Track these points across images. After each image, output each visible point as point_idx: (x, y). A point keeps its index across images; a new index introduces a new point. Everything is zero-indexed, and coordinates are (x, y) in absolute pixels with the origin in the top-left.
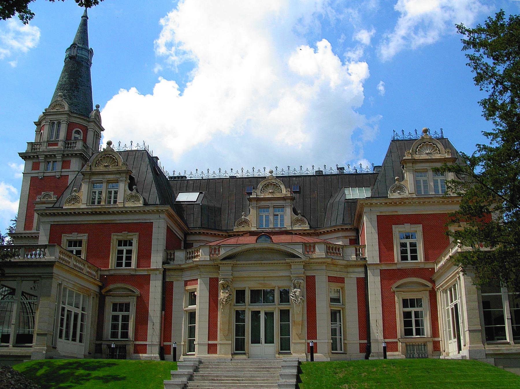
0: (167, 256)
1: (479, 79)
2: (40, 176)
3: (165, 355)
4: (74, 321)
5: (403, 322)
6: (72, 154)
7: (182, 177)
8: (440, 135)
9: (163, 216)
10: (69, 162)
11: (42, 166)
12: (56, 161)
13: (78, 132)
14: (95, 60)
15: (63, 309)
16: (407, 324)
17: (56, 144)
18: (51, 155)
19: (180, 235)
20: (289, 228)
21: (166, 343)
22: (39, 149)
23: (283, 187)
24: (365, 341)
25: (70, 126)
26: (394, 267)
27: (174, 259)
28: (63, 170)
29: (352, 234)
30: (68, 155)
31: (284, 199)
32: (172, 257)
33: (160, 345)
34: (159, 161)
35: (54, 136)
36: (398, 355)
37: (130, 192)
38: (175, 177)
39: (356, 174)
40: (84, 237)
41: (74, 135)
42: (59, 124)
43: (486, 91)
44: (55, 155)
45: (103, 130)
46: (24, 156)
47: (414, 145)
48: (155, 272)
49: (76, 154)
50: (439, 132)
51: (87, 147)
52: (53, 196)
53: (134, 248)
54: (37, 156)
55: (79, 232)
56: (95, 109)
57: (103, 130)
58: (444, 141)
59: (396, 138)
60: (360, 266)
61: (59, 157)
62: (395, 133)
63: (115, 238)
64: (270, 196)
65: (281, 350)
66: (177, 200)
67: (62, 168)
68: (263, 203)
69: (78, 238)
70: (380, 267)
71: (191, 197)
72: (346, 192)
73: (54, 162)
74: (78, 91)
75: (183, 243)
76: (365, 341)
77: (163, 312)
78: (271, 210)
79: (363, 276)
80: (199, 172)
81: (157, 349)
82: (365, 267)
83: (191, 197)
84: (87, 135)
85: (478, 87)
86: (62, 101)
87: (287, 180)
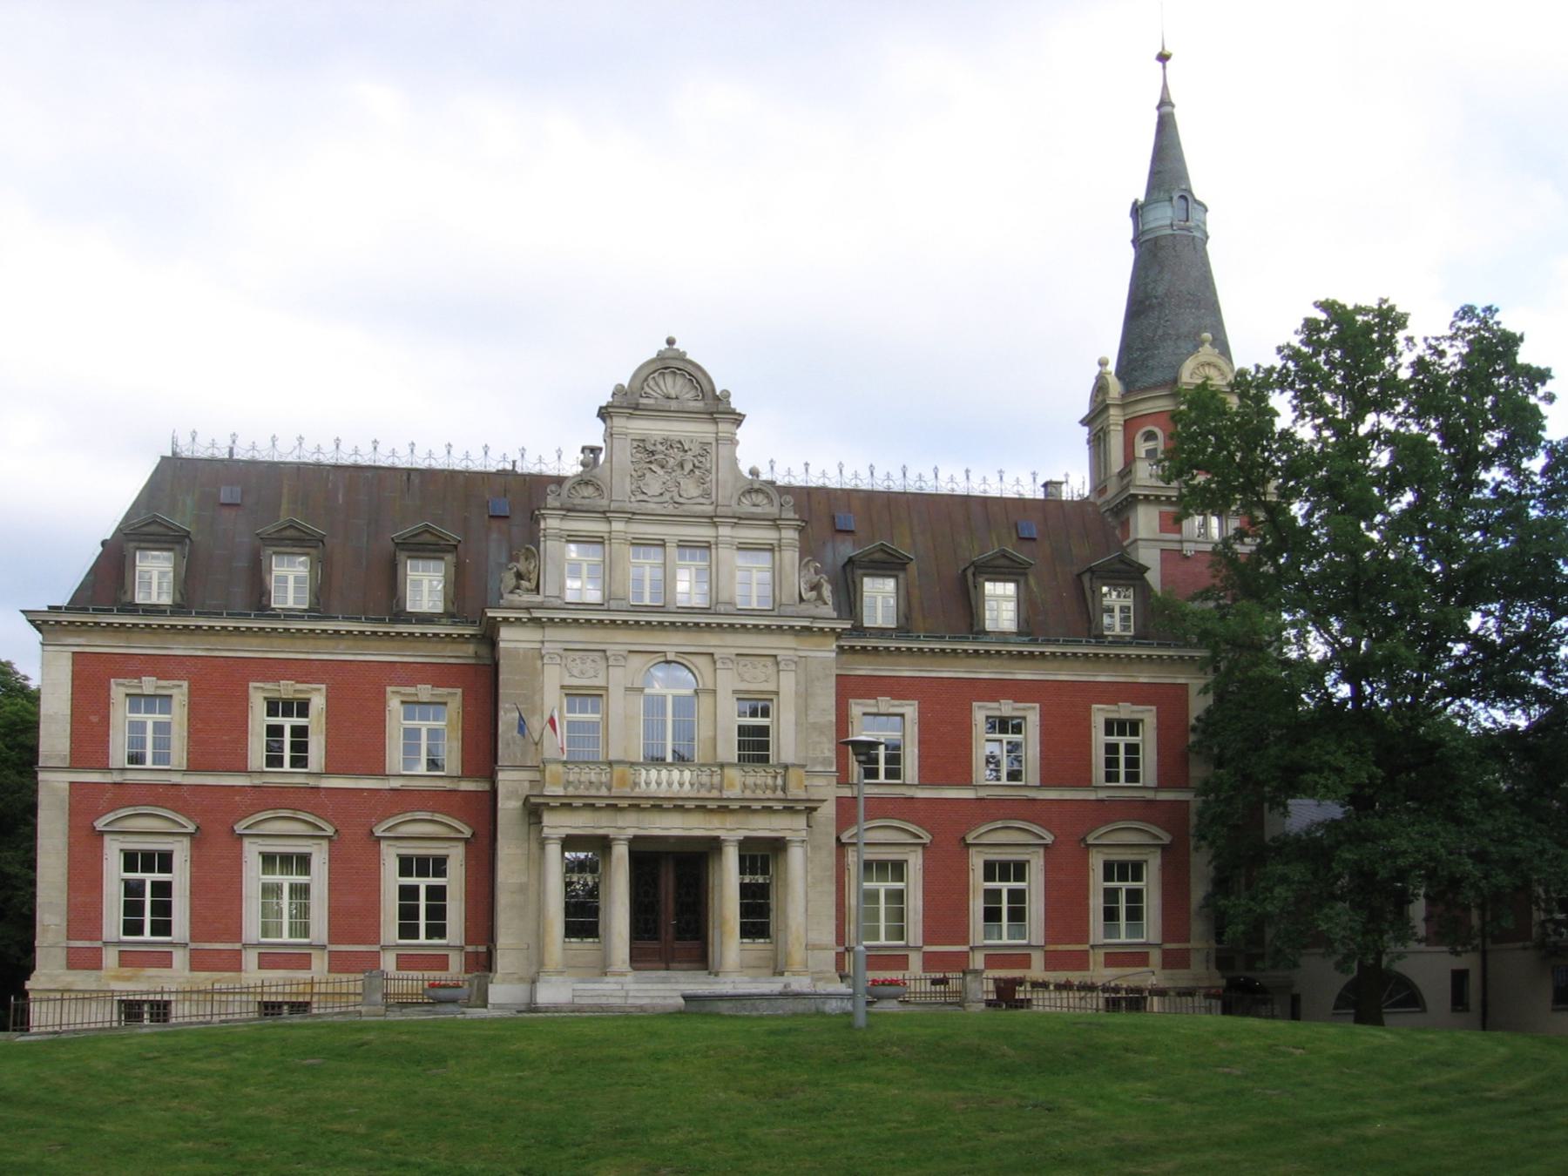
26: (1092, 796)
63: (980, 714)
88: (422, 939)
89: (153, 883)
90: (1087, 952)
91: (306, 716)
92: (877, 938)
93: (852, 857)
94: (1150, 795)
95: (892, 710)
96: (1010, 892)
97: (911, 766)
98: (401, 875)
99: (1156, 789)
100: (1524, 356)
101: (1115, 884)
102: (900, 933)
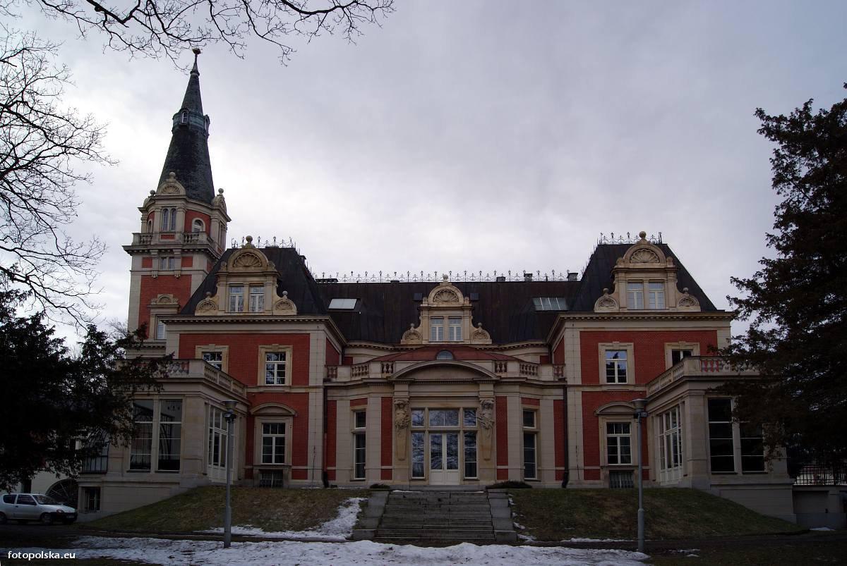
0: (383, 368)
1: (778, 181)
2: (155, 274)
3: (329, 481)
4: (215, 444)
5: (708, 426)
6: (194, 250)
7: (333, 280)
8: (658, 240)
9: (322, 327)
10: (192, 258)
11: (156, 264)
12: (173, 258)
13: (199, 222)
14: (212, 130)
15: (211, 431)
16: (612, 450)
17: (173, 237)
18: (166, 250)
19: (338, 348)
20: (467, 342)
21: (329, 468)
22: (150, 241)
23: (460, 295)
24: (563, 468)
25: (189, 215)
26: (598, 389)
27: (336, 376)
28: (183, 269)
29: (544, 351)
30: (189, 250)
31: (462, 308)
32: (334, 373)
33: (323, 470)
34: (306, 261)
35: (168, 226)
36: (600, 484)
37: (279, 298)
38: (324, 280)
39: (547, 283)
40: (224, 350)
41: (195, 226)
42: (174, 210)
43: (788, 193)
44: (171, 250)
45: (229, 220)
46: (129, 250)
47: (630, 251)
48: (314, 390)
49: (200, 250)
50: (657, 236)
51: (210, 240)
52: (172, 300)
53: (288, 362)
54: (149, 250)
55: (217, 344)
56: (218, 193)
57: (229, 220)
58: (665, 249)
59: (603, 242)
60: (558, 387)
61: (177, 253)
62: (603, 236)
63: (262, 350)
64: (445, 305)
65: (466, 476)
66: (330, 307)
67: (182, 266)
68: (436, 313)
69: (216, 351)
70: (582, 389)
71: (350, 304)
72: (536, 302)
73: (170, 258)
74: (195, 171)
75: (340, 356)
76: (563, 468)
77: (326, 434)
78: (446, 321)
79: (562, 398)
80: (355, 275)
81: (319, 474)
82: (565, 388)
83: (350, 304)
84: (210, 226)
85: (776, 190)
86: (175, 183)
87: (466, 288)
88: (619, 463)
89: (276, 438)
90: (294, 464)
91: (284, 360)
92: (617, 463)
93: (259, 423)
94: (631, 389)
95: (621, 348)
96: (621, 438)
97: (630, 378)
98: (608, 433)
99: (635, 386)
100: (774, 157)
101: (270, 435)
102: (280, 459)
